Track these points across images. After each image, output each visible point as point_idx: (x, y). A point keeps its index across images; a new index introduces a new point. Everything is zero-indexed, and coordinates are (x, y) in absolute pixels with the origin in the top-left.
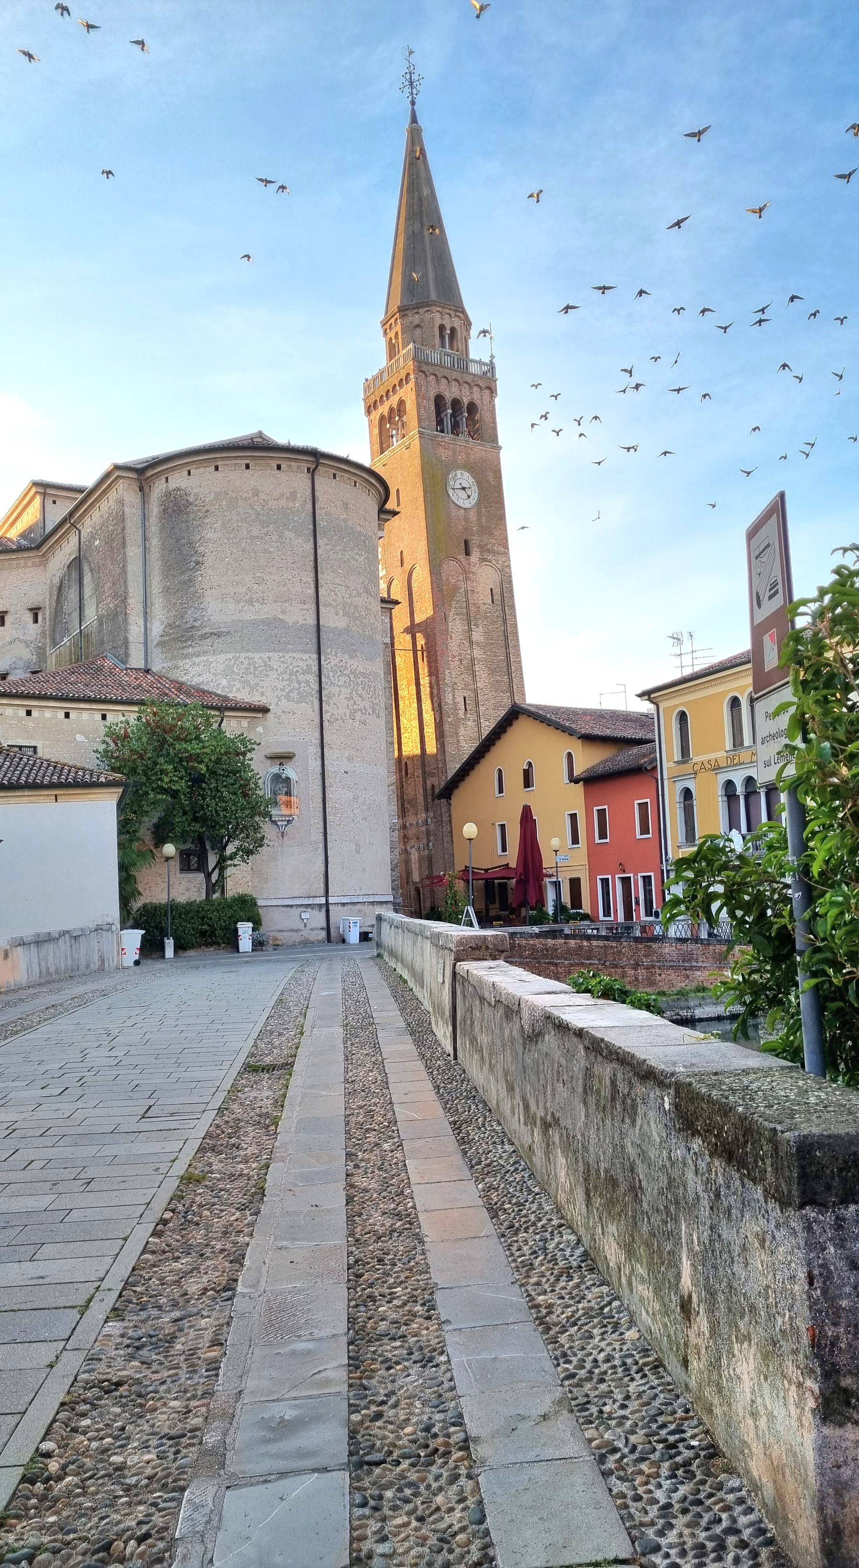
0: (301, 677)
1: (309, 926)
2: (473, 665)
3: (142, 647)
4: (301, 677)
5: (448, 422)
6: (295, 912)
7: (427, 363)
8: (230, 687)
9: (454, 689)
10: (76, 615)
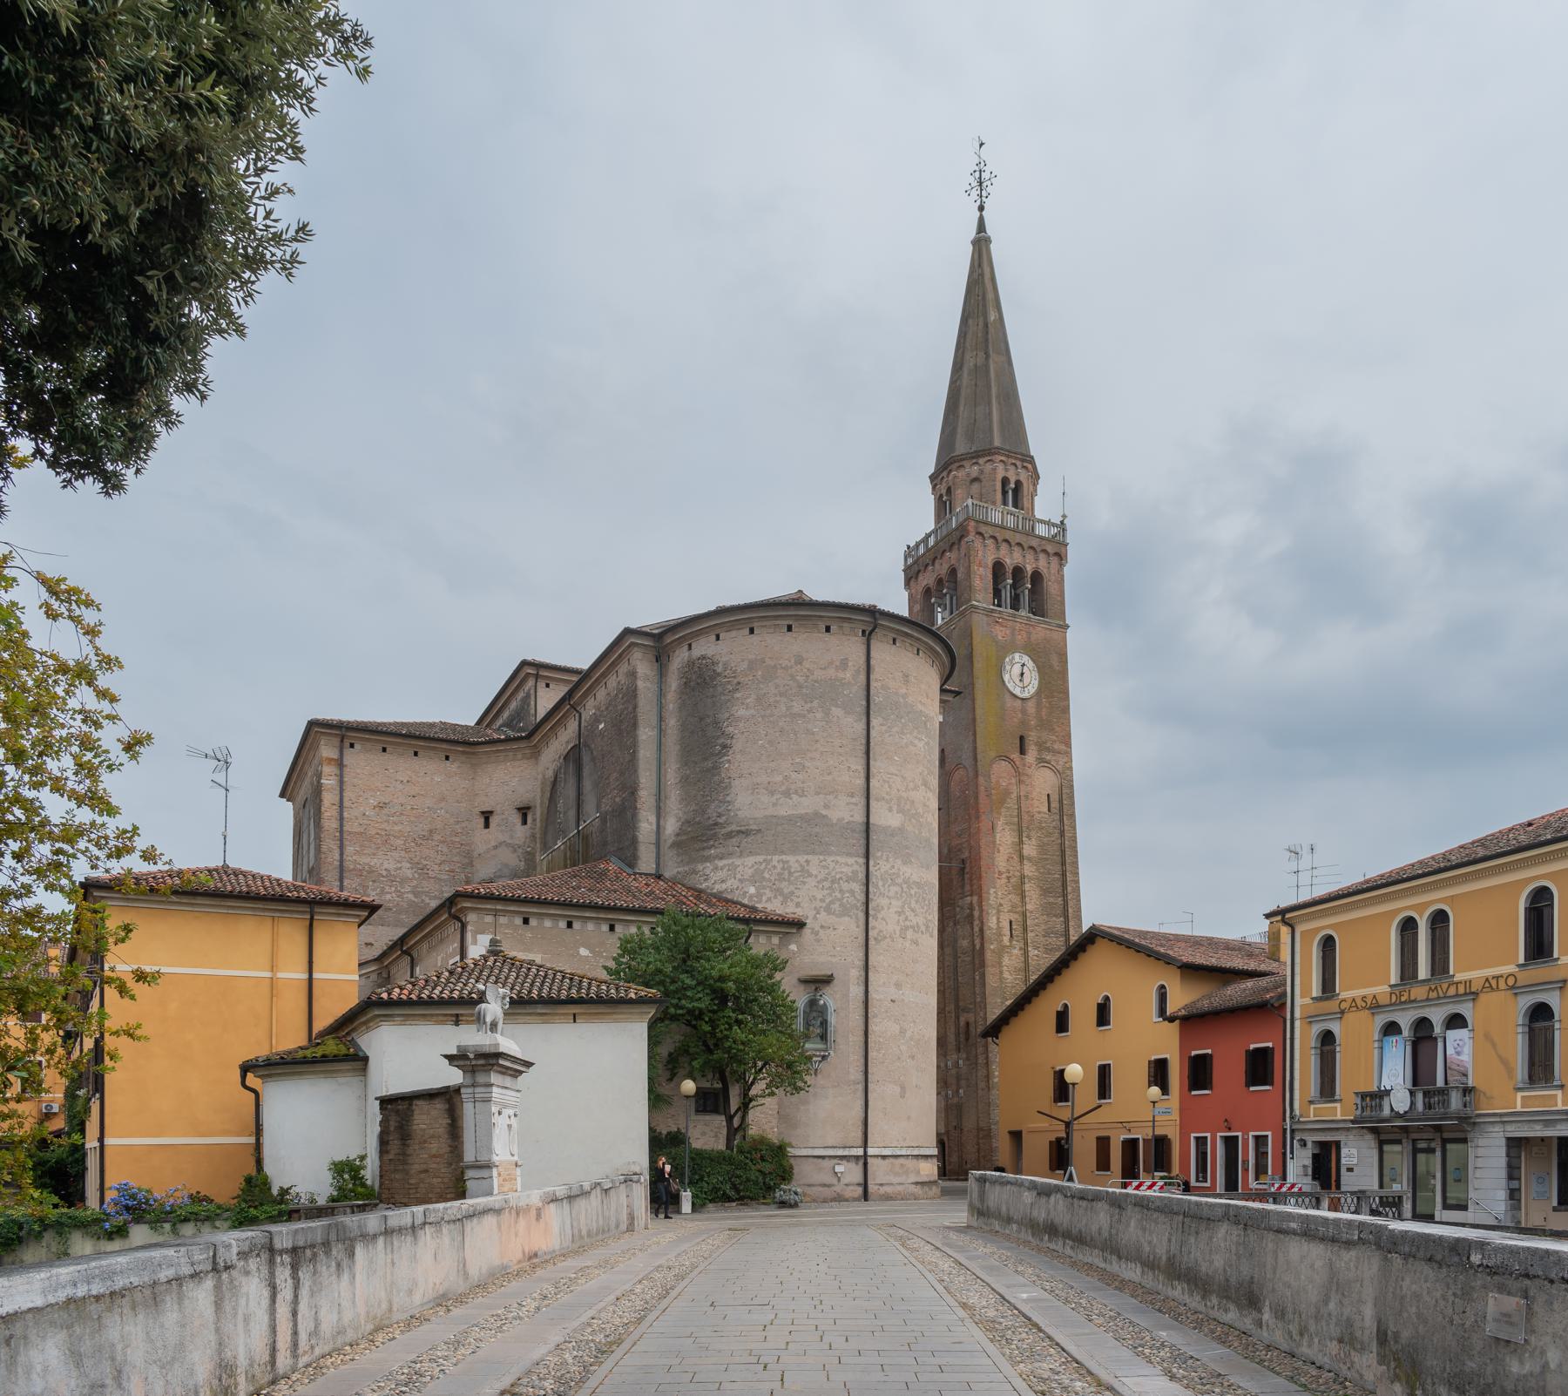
0: (845, 886)
1: (845, 1180)
2: (1023, 883)
3: (653, 848)
4: (845, 886)
5: (1006, 595)
6: (827, 1163)
7: (986, 523)
8: (759, 895)
9: (999, 912)
10: (572, 813)
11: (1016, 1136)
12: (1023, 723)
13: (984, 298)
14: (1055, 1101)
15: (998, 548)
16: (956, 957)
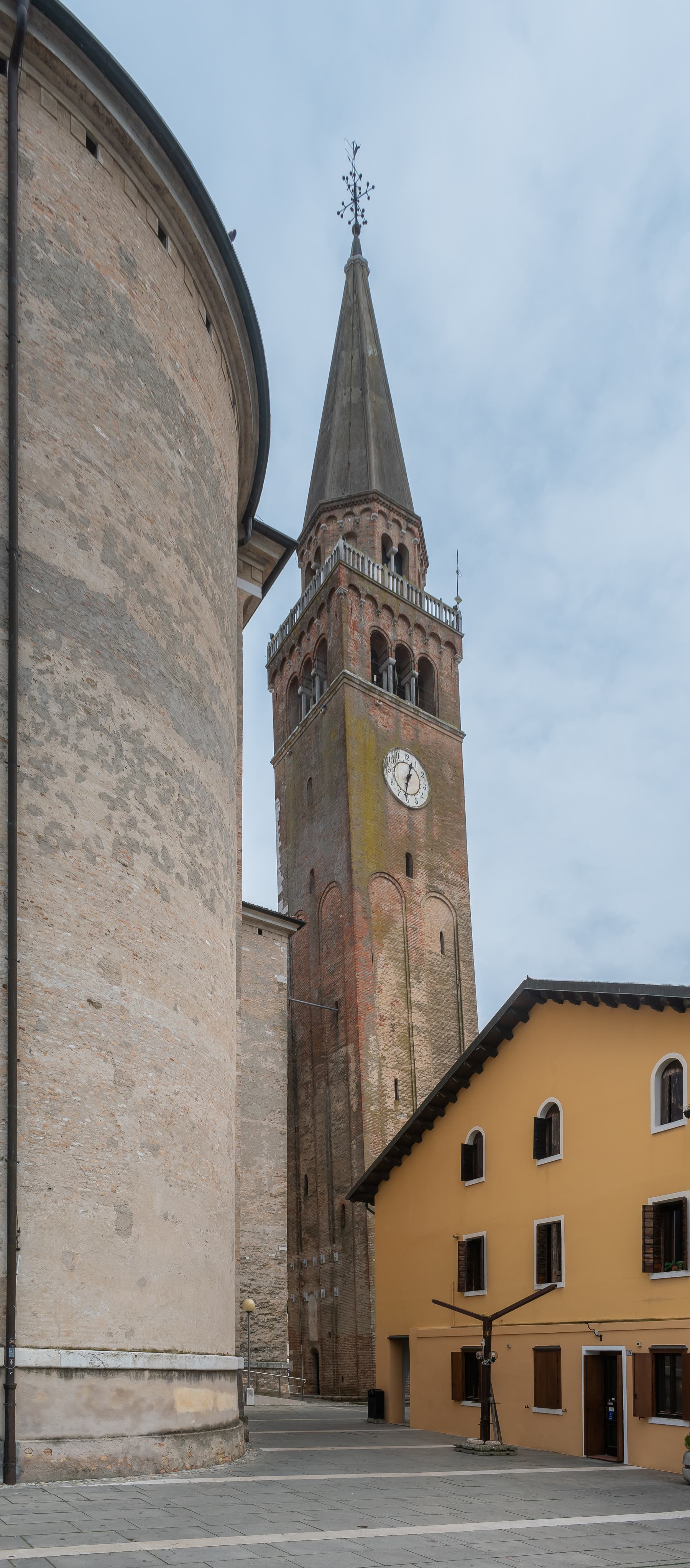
2: (411, 1035)
5: (389, 678)
7: (362, 576)
11: (401, 1344)
12: (410, 838)
13: (360, 328)
14: (461, 1289)
15: (378, 614)
16: (329, 1125)
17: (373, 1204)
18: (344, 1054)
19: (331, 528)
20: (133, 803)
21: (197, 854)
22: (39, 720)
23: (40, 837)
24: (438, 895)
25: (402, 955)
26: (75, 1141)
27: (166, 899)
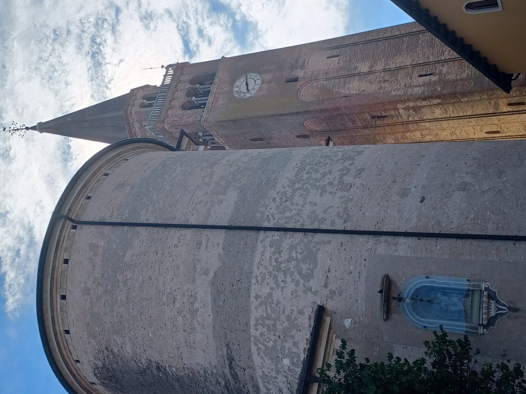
0: (285, 256)
2: (390, 70)
4: (285, 256)
17: (512, 75)
18: (403, 110)
19: (139, 134)
20: (321, 183)
21: (337, 158)
22: (294, 220)
23: (344, 221)
24: (306, 62)
25: (342, 80)
26: (501, 209)
27: (363, 170)
